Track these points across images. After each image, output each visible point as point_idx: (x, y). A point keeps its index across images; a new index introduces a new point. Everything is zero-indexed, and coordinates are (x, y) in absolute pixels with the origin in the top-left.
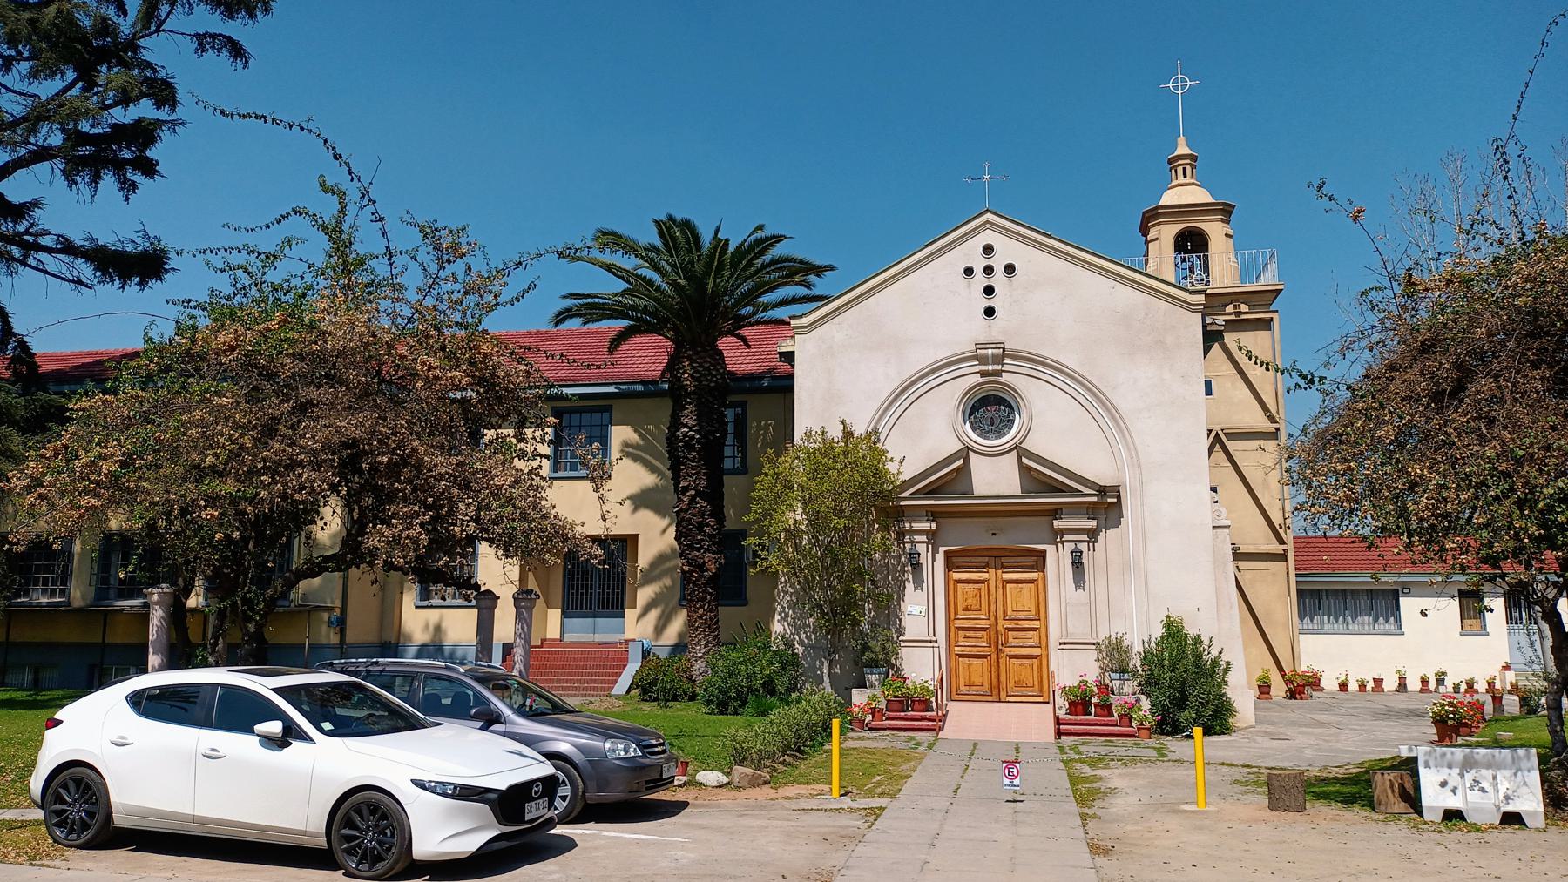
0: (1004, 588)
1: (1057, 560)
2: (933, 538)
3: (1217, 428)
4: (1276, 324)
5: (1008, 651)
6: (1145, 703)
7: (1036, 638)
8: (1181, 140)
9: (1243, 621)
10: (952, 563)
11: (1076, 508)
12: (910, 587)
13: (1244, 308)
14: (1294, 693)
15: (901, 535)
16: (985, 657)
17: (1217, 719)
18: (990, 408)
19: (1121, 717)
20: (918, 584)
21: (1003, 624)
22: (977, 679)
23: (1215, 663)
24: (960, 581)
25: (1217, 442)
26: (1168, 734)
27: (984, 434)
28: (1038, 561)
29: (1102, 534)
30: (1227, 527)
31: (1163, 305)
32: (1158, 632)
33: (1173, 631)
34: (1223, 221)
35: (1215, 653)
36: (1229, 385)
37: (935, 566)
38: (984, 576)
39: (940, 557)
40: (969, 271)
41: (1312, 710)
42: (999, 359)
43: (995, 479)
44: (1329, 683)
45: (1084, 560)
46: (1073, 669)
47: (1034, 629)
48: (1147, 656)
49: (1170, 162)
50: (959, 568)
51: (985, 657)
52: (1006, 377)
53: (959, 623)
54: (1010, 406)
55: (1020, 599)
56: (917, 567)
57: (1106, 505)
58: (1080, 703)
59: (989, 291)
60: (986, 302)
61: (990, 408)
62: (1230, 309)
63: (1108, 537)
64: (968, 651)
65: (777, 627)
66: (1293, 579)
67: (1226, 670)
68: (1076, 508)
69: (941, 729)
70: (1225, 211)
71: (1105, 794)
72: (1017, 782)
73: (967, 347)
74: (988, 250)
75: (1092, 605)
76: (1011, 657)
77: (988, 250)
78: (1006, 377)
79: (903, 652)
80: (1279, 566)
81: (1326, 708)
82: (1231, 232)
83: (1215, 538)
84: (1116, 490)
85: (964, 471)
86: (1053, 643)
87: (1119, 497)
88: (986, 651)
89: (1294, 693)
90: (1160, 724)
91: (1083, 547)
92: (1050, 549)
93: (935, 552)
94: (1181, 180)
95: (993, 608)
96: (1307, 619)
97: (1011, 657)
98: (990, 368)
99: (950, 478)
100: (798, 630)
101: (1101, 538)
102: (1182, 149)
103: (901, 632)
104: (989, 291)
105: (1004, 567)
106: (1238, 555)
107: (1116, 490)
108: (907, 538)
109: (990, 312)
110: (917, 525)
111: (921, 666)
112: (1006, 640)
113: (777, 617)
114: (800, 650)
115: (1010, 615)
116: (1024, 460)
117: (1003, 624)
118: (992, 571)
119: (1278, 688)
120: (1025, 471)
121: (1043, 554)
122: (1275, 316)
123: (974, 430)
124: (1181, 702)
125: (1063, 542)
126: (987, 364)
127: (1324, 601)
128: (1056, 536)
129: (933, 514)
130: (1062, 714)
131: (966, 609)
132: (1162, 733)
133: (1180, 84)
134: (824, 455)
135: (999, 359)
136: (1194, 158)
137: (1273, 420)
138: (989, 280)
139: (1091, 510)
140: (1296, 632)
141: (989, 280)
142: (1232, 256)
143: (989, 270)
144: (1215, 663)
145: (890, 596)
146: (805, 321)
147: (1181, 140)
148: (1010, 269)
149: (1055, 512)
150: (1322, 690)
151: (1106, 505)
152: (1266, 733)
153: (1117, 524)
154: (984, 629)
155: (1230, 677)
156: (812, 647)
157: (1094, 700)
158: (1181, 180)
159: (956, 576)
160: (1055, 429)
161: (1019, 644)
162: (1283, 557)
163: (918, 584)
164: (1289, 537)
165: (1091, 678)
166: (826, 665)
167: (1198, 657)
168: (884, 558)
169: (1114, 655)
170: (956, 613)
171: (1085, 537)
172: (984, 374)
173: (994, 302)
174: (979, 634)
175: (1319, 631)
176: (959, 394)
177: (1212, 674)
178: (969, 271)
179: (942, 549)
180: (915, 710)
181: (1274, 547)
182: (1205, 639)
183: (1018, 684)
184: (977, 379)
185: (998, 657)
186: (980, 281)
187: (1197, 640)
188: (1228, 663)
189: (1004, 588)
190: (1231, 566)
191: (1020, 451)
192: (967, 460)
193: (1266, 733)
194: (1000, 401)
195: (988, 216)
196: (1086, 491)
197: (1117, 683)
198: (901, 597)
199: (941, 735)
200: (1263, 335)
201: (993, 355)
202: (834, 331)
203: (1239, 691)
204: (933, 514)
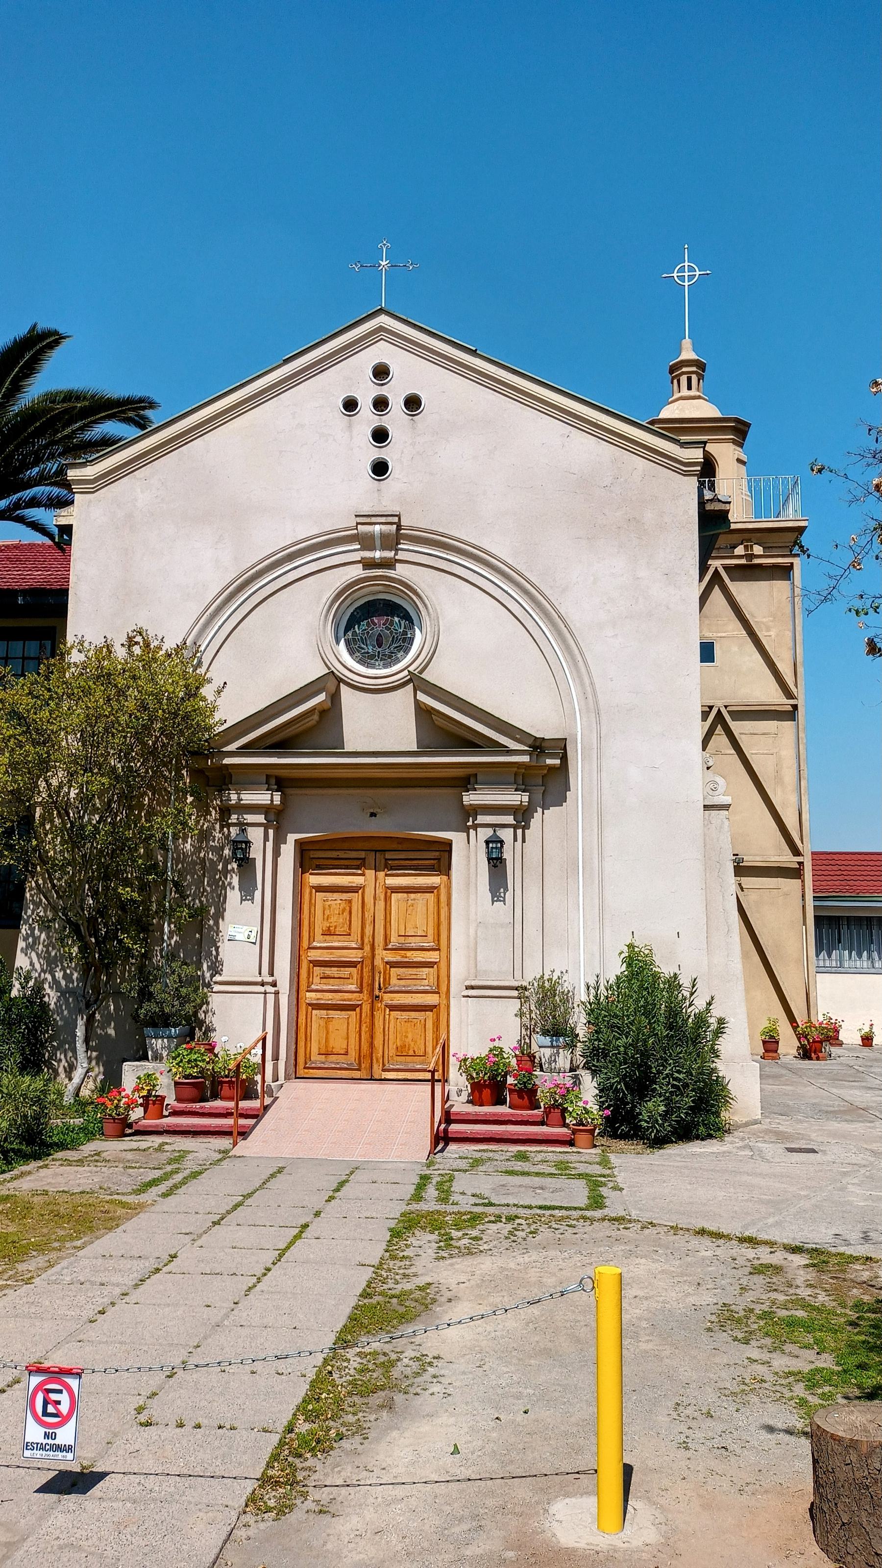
0: (387, 900)
1: (468, 853)
2: (277, 820)
3: (719, 704)
4: (797, 572)
5: (388, 998)
6: (589, 1088)
7: (432, 980)
8: (687, 343)
9: (745, 955)
10: (308, 858)
11: (492, 775)
12: (233, 896)
13: (758, 550)
14: (808, 1052)
15: (225, 811)
16: (352, 1008)
17: (698, 1114)
18: (377, 619)
19: (548, 1110)
20: (248, 890)
21: (383, 956)
22: (338, 1044)
23: (701, 1020)
24: (320, 889)
25: (719, 722)
26: (624, 1137)
27: (366, 660)
28: (438, 858)
29: (538, 815)
30: (726, 807)
31: (640, 464)
32: (615, 969)
33: (638, 967)
34: (734, 442)
35: (700, 1004)
36: (735, 649)
37: (277, 864)
38: (358, 880)
39: (288, 851)
40: (350, 405)
41: (835, 1079)
42: (392, 541)
43: (378, 726)
44: (850, 1036)
45: (507, 855)
46: (482, 1029)
47: (429, 965)
48: (597, 1012)
49: (672, 370)
50: (321, 867)
51: (352, 1008)
52: (401, 571)
53: (314, 955)
54: (407, 617)
55: (410, 917)
56: (246, 864)
57: (544, 771)
58: (489, 1085)
59: (380, 436)
60: (374, 453)
61: (377, 619)
62: (740, 550)
63: (546, 820)
64: (328, 999)
65: (21, 961)
66: (809, 895)
67: (719, 1032)
68: (492, 775)
69: (244, 1134)
70: (739, 431)
71: (708, 1010)
72: (65, 1435)
73: (344, 521)
74: (381, 372)
75: (518, 923)
76: (393, 1008)
77: (381, 372)
78: (401, 571)
79: (215, 1001)
80: (793, 884)
81: (855, 1076)
82: (744, 458)
83: (707, 823)
84: (560, 747)
85: (329, 716)
86: (456, 987)
87: (564, 758)
88: (354, 999)
89: (808, 1052)
90: (610, 1122)
91: (506, 835)
92: (457, 838)
93: (279, 841)
94: (685, 392)
95: (368, 930)
96: (824, 954)
97: (393, 1008)
98: (378, 554)
99: (309, 720)
100: (51, 963)
101: (536, 821)
102: (688, 354)
103: (216, 969)
104: (380, 436)
105: (391, 867)
106: (741, 870)
107: (560, 747)
108: (234, 818)
109: (380, 468)
110: (250, 797)
111: (238, 1024)
112: (387, 981)
113: (21, 944)
114: (51, 997)
115: (394, 941)
116: (421, 697)
117: (383, 956)
118: (370, 873)
119: (789, 1045)
120: (423, 713)
121: (447, 846)
122: (796, 561)
123: (351, 652)
124: (642, 1085)
125: (475, 827)
126: (373, 548)
127: (844, 930)
128: (466, 819)
129: (279, 781)
130: (460, 1105)
131: (328, 933)
132: (615, 1136)
133: (686, 273)
134: (102, 673)
135: (392, 541)
136: (701, 366)
137: (789, 695)
138: (383, 416)
139: (520, 778)
140: (812, 969)
141: (383, 416)
142: (744, 482)
143: (381, 404)
144: (701, 1020)
145: (203, 910)
146: (90, 471)
147: (687, 343)
148: (413, 403)
149: (467, 780)
150: (841, 1044)
151: (544, 771)
152: (780, 1136)
153: (561, 800)
154: (352, 964)
155: (724, 1045)
156: (73, 992)
157: (510, 1080)
158: (685, 392)
159: (314, 880)
160: (474, 653)
161: (402, 987)
162: (796, 873)
163: (248, 890)
164: (807, 848)
165: (509, 1043)
166: (81, 1023)
167: (674, 1013)
168: (199, 849)
169: (547, 1009)
170: (312, 938)
171: (510, 819)
172: (369, 564)
173: (387, 453)
174: (345, 972)
175: (839, 970)
176: (328, 594)
177: (696, 1039)
178: (350, 405)
179: (292, 838)
180: (224, 1094)
181: (787, 859)
182: (685, 981)
183: (402, 1051)
184: (357, 572)
185: (366, 1011)
186: (368, 417)
187: (673, 983)
188: (721, 1021)
189: (387, 900)
190: (731, 879)
191: (416, 681)
192: (335, 697)
193: (780, 1136)
194: (391, 609)
195: (383, 320)
196: (513, 745)
197: (548, 1052)
198: (220, 914)
199: (244, 1147)
200: (780, 587)
201: (383, 535)
202: (139, 491)
203: (737, 1065)
204: (279, 781)
